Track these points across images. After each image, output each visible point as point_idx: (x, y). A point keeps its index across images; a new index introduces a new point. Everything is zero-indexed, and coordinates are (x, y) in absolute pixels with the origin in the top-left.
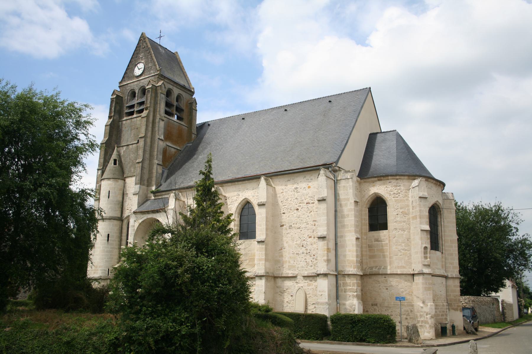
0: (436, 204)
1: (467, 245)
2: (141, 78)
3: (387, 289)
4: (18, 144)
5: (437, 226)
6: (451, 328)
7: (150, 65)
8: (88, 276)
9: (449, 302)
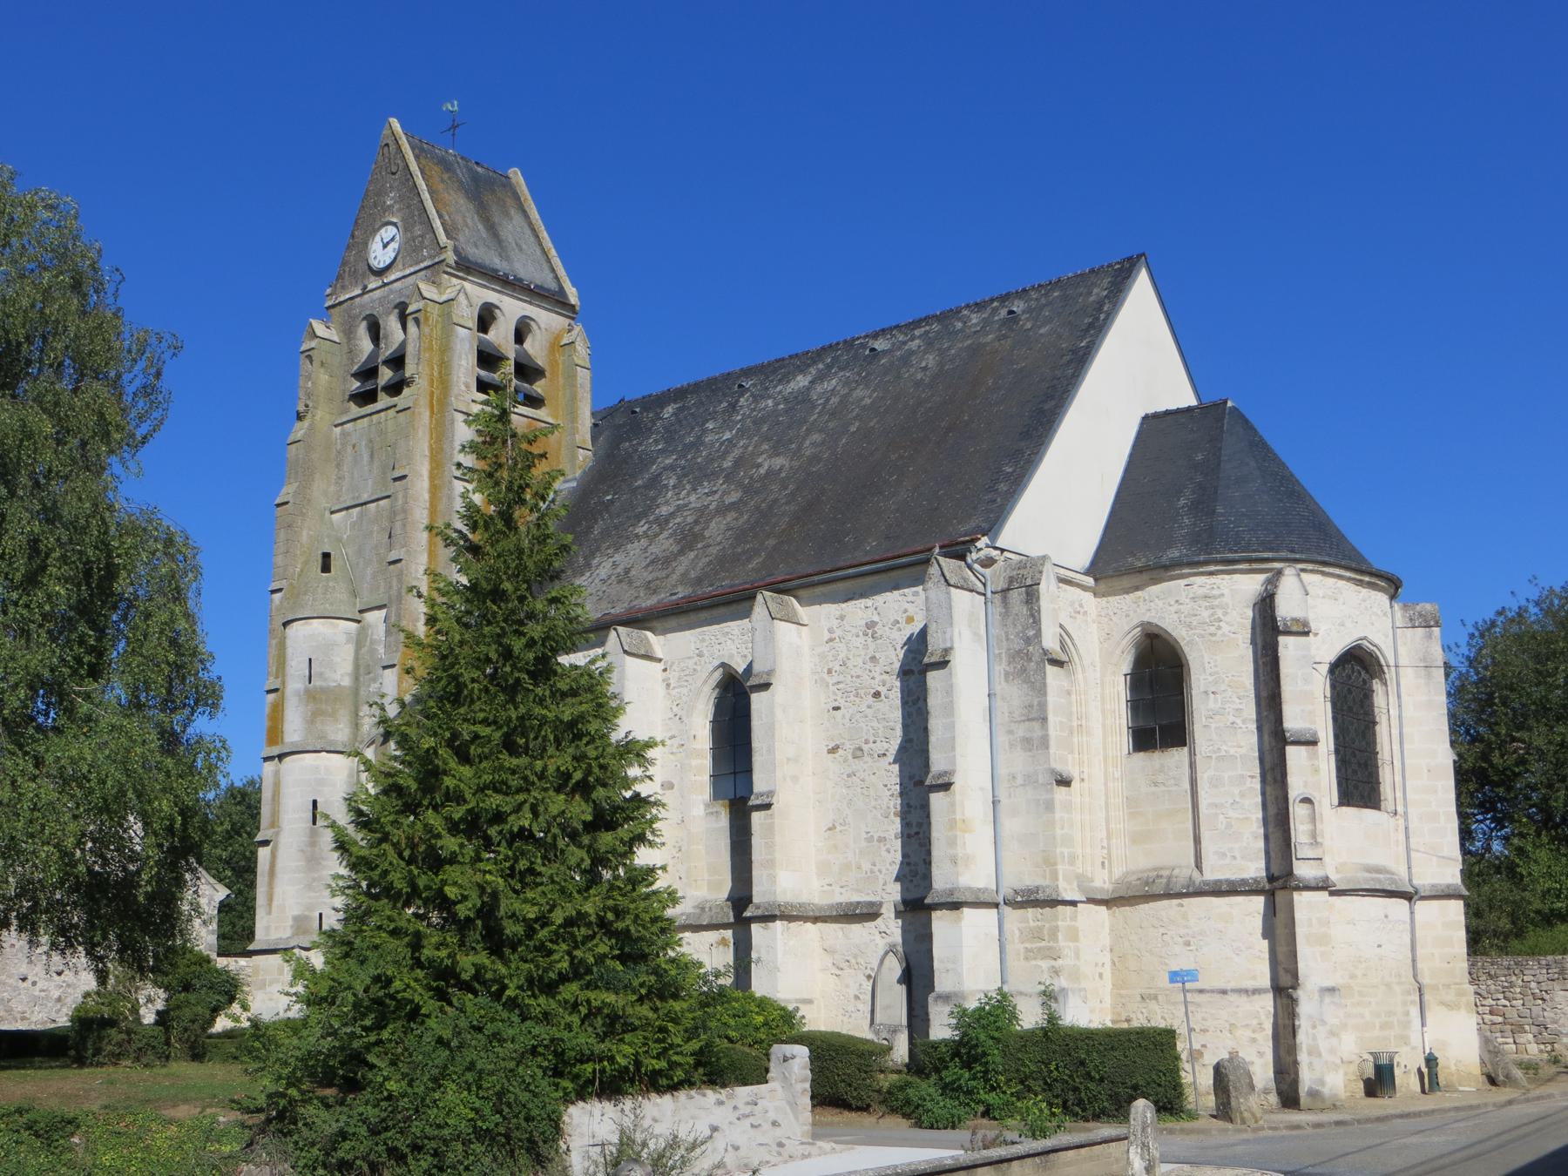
2: (393, 277)
3: (1188, 944)
5: (1375, 723)
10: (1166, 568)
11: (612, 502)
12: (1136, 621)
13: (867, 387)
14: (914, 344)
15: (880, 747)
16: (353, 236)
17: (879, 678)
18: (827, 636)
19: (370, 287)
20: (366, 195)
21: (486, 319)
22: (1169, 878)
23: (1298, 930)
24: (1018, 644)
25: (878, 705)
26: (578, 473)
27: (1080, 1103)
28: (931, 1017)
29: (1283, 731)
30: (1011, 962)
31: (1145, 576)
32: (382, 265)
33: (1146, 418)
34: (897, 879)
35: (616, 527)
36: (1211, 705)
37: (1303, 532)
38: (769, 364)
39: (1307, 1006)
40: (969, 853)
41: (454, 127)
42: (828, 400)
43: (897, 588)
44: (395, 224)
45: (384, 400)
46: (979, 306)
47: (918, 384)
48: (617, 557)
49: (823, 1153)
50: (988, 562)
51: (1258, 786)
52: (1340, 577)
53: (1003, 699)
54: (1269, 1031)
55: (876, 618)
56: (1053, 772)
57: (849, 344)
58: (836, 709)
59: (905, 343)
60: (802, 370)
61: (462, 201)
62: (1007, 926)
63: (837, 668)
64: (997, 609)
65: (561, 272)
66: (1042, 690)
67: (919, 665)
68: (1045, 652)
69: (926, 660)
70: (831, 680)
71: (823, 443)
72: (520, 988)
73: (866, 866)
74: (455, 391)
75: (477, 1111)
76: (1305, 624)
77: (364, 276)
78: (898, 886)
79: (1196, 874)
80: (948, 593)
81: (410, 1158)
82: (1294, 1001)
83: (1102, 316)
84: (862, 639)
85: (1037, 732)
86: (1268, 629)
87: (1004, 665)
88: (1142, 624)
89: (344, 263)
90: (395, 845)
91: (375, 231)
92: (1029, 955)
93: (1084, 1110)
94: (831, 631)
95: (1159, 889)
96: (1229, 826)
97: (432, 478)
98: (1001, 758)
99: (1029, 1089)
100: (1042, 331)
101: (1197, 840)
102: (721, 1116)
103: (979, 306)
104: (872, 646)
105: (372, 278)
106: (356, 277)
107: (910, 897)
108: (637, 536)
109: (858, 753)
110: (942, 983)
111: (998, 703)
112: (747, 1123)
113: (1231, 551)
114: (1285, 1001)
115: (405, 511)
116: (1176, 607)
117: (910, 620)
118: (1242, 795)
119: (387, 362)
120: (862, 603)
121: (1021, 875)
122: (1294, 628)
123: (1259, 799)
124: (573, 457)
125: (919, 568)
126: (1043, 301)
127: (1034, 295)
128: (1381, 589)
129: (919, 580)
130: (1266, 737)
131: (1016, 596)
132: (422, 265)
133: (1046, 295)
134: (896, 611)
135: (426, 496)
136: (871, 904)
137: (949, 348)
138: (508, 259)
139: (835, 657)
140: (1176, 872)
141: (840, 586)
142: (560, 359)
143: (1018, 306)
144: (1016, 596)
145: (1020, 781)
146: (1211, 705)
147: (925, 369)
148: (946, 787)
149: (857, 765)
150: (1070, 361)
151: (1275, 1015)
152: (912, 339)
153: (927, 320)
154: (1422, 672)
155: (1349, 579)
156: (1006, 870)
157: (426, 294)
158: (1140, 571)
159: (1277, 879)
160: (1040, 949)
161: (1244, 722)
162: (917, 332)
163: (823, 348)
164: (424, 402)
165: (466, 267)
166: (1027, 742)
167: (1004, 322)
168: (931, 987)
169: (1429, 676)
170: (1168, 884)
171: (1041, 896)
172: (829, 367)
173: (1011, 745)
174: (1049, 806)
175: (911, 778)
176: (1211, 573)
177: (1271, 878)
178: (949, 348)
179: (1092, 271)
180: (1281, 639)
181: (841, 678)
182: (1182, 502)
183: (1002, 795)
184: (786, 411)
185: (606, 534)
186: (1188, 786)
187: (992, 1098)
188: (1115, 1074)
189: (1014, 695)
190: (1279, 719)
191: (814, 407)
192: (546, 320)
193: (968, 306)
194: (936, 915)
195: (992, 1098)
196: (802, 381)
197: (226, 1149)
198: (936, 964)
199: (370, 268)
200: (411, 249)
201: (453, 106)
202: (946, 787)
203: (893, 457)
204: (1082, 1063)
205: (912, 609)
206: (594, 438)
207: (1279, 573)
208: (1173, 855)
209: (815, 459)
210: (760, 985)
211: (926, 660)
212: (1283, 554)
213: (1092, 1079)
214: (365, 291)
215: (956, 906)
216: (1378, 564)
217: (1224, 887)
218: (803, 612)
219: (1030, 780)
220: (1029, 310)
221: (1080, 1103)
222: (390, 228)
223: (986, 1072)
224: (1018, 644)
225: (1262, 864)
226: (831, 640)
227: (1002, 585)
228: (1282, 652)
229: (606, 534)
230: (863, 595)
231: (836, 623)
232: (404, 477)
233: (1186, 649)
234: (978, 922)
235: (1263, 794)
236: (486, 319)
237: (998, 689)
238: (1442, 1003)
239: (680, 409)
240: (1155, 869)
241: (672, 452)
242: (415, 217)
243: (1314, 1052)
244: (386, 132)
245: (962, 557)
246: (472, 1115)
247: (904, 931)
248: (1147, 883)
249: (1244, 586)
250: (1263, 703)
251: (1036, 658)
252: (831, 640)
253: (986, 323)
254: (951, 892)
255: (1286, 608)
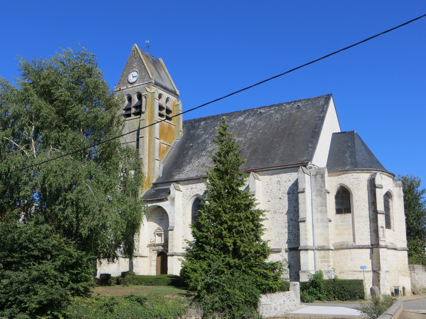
0: (388, 191)
1: (311, 142)
2: (136, 85)
3: (352, 260)
4: (214, 216)
5: (389, 209)
6: (402, 289)
7: (143, 74)
8: (178, 274)
9: (399, 270)
10: (347, 171)
11: (192, 146)
12: (338, 183)
13: (261, 121)
14: (272, 111)
15: (281, 211)
16: (123, 73)
17: (281, 194)
18: (266, 183)
19: (129, 87)
20: (127, 63)
21: (160, 96)
22: (347, 244)
23: (381, 257)
24: (319, 188)
25: (281, 201)
26: (180, 138)
27: (342, 297)
28: (300, 276)
29: (377, 211)
30: (317, 264)
31: (341, 172)
32: (132, 82)
33: (333, 134)
34: (287, 243)
35: (196, 153)
36: (358, 204)
37: (373, 164)
38: (230, 113)
39: (382, 275)
40: (307, 237)
41: (148, 47)
42: (250, 124)
43: (286, 173)
44: (137, 72)
45: (133, 117)
46: (288, 103)
47: (276, 122)
48: (199, 160)
49: (303, 307)
50: (311, 168)
51: (369, 223)
52: (385, 175)
53: (315, 201)
54: (371, 281)
55: (280, 180)
56: (328, 219)
57: (253, 110)
58: (269, 201)
59: (269, 111)
60: (240, 115)
61: (152, 66)
62: (316, 255)
63: (269, 191)
64: (313, 179)
65: (175, 86)
66: (325, 199)
67: (294, 193)
68: (326, 190)
69: (299, 191)
70: (267, 194)
71: (253, 135)
72: (245, 267)
73: (277, 240)
74: (155, 116)
75: (245, 296)
76: (382, 186)
77: (126, 84)
78: (287, 245)
79: (354, 244)
80: (304, 175)
81: (233, 307)
82: (379, 274)
83: (325, 109)
84: (276, 185)
85: (324, 209)
86: (372, 187)
87: (315, 192)
88: (340, 184)
89: (120, 80)
90: (211, 233)
91: (130, 73)
92: (322, 262)
93: (343, 298)
94: (267, 182)
95: (345, 246)
96: (362, 232)
97: (149, 137)
98: (314, 215)
99: (330, 293)
100: (308, 111)
101: (354, 235)
102: (284, 298)
103: (288, 103)
104: (279, 186)
105: (129, 85)
106: (124, 84)
107: (289, 247)
108: (203, 155)
109: (275, 212)
110: (303, 268)
111: (313, 202)
112: (289, 300)
113: (362, 167)
114: (376, 274)
115: (143, 146)
116: (349, 180)
117: (290, 181)
118: (365, 225)
119: (133, 107)
120: (276, 176)
121: (320, 242)
122: (380, 187)
123: (369, 226)
124: (179, 134)
125: (296, 168)
126: (306, 103)
127: (303, 102)
128: (391, 177)
129: (297, 171)
130: (371, 212)
131: (319, 177)
132: (145, 83)
133: (307, 102)
134: (287, 179)
135: (148, 142)
136: (279, 249)
137: (283, 113)
138: (163, 82)
139: (269, 189)
140: (348, 243)
141: (271, 171)
142: (175, 109)
143: (300, 104)
144: (319, 177)
145: (319, 220)
146: (358, 204)
147: (277, 118)
148: (304, 221)
149: (275, 215)
150: (319, 120)
151: (373, 277)
152: (271, 110)
153: (274, 105)
154: (398, 197)
155: (387, 175)
156: (315, 242)
157: (148, 91)
158: (340, 171)
159: (374, 245)
160: (325, 261)
161: (365, 208)
162: (272, 108)
163: (245, 110)
164: (147, 118)
165: (157, 84)
166: (321, 211)
167: (297, 108)
168: (300, 270)
169: (400, 199)
170: (347, 246)
171: (325, 248)
172: (248, 115)
173: (317, 212)
174: (327, 227)
175: (290, 219)
176: (358, 173)
177: (372, 245)
178: (283, 113)
179: (318, 97)
180: (377, 189)
181: (270, 194)
182: (347, 155)
183: (315, 224)
184: (239, 126)
185: (193, 154)
186: (351, 222)
187: (321, 295)
188: (345, 291)
189: (318, 200)
190: (375, 207)
191: (247, 126)
192: (173, 98)
193: (285, 103)
194: (301, 252)
195: (321, 295)
196: (241, 119)
197: (185, 305)
198: (301, 264)
199: (128, 82)
200: (141, 78)
201: (148, 42)
202: (304, 221)
203: (276, 140)
204: (343, 287)
205: (290, 178)
206: (183, 128)
207: (376, 174)
208: (347, 239)
209: (251, 139)
210: (134, 271)
211: (299, 191)
212: (375, 169)
213: (345, 291)
214: (127, 88)
215: (307, 250)
216: (389, 171)
217: (361, 247)
218: (260, 177)
219: (322, 220)
220: (303, 105)
221: (342, 297)
222: (135, 72)
223: (320, 289)
224: (319, 188)
225: (370, 242)
226: (268, 184)
227: (314, 174)
228: (377, 192)
229: (193, 154)
230: (276, 174)
231: (269, 180)
232: (143, 137)
233: (352, 190)
234: (311, 253)
235: (370, 225)
236: (160, 96)
237: (313, 198)
238: (403, 275)
239: (206, 123)
240: (343, 242)
241: (207, 134)
242: (143, 70)
243: (384, 286)
244: (133, 47)
245: (305, 166)
246: (244, 297)
247: (288, 256)
248: (341, 245)
249: (365, 176)
250: (370, 204)
251: (324, 191)
252: (268, 184)
253: (292, 108)
254: (306, 246)
255: (378, 181)
